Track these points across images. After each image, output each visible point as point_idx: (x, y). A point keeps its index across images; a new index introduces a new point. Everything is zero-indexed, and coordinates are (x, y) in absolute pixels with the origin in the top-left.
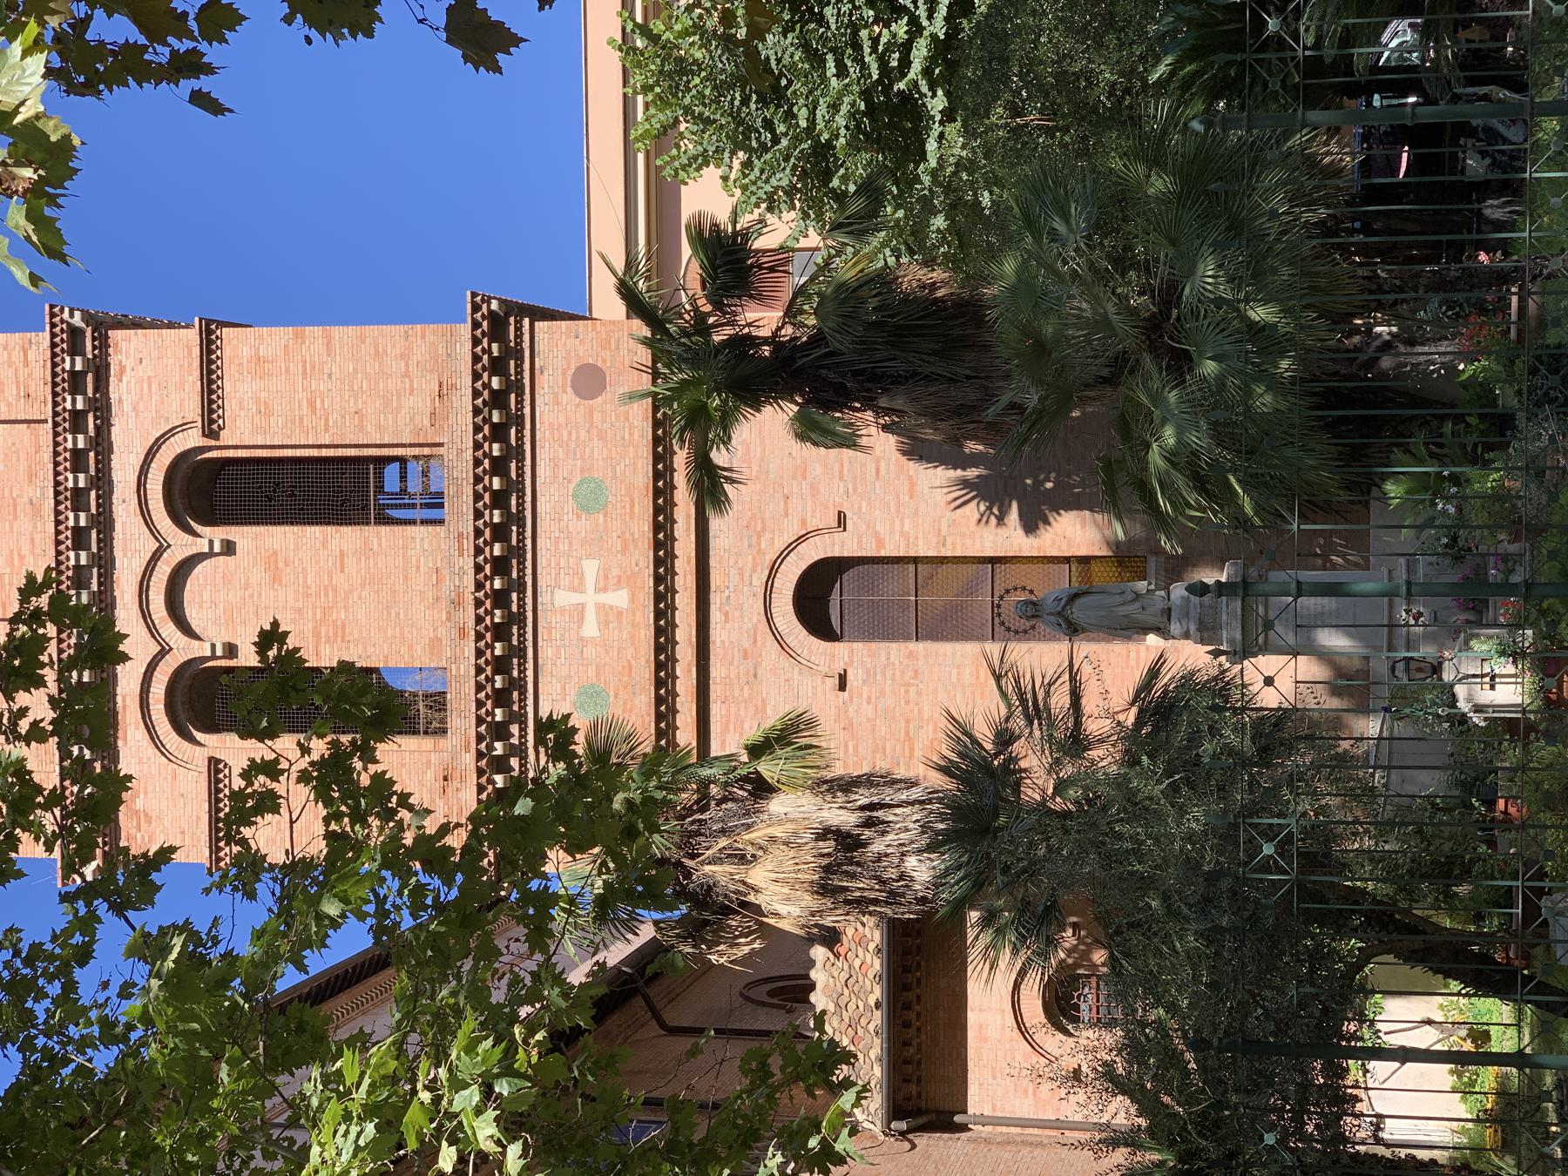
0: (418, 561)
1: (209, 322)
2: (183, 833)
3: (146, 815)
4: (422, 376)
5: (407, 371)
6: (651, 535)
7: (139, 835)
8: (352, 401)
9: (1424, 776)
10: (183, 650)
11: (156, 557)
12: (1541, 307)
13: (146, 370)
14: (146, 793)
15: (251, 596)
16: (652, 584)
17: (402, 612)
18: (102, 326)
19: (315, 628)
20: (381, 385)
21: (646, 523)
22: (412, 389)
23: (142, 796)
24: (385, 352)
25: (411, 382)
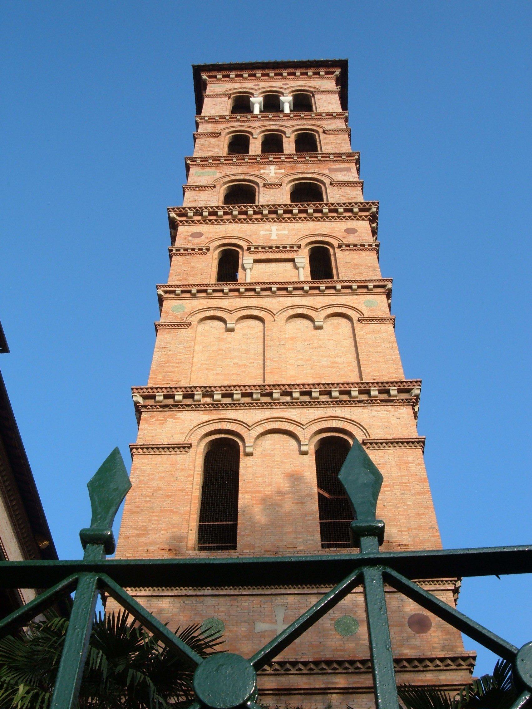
0: (300, 538)
1: (423, 442)
2: (153, 436)
3: (164, 423)
4: (410, 537)
5: (412, 529)
6: (323, 659)
7: (154, 420)
8: (390, 504)
9: (203, 181)
10: (249, 436)
11: (299, 424)
12: (407, 601)
13: (394, 421)
14: (175, 422)
15: (278, 464)
16: (290, 660)
17: (269, 531)
18: (414, 402)
19: (261, 491)
20: (402, 517)
21: (280, 265)
22: (401, 531)
23: (174, 421)
24: (422, 518)
25: (406, 531)
